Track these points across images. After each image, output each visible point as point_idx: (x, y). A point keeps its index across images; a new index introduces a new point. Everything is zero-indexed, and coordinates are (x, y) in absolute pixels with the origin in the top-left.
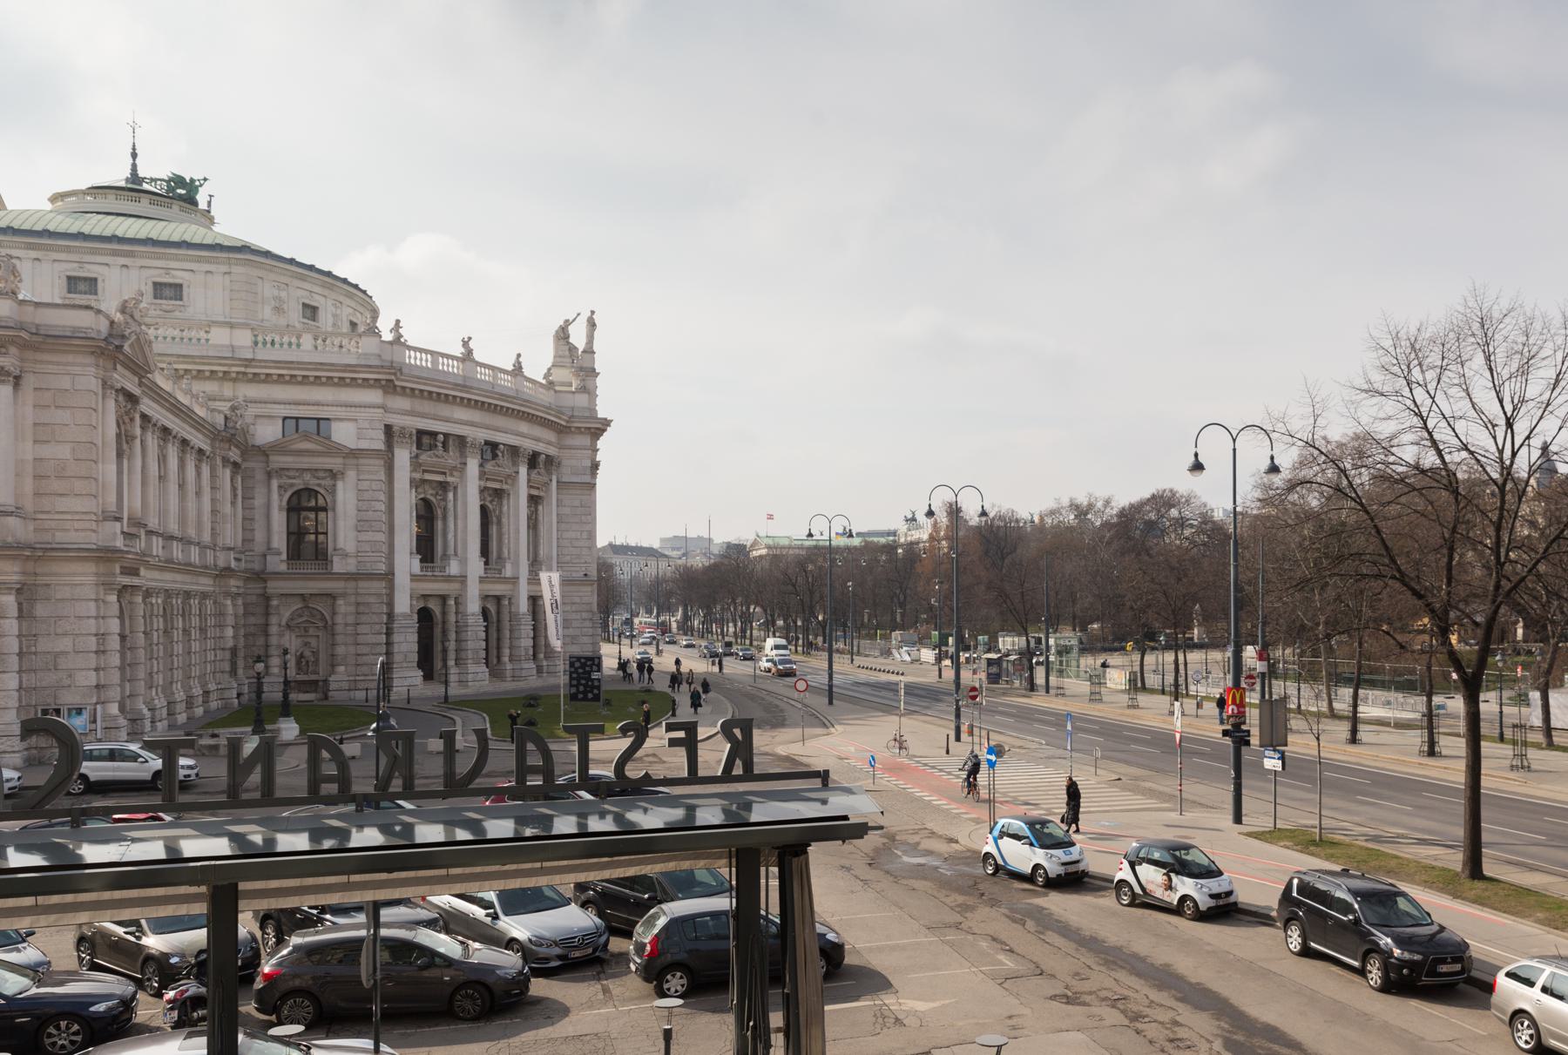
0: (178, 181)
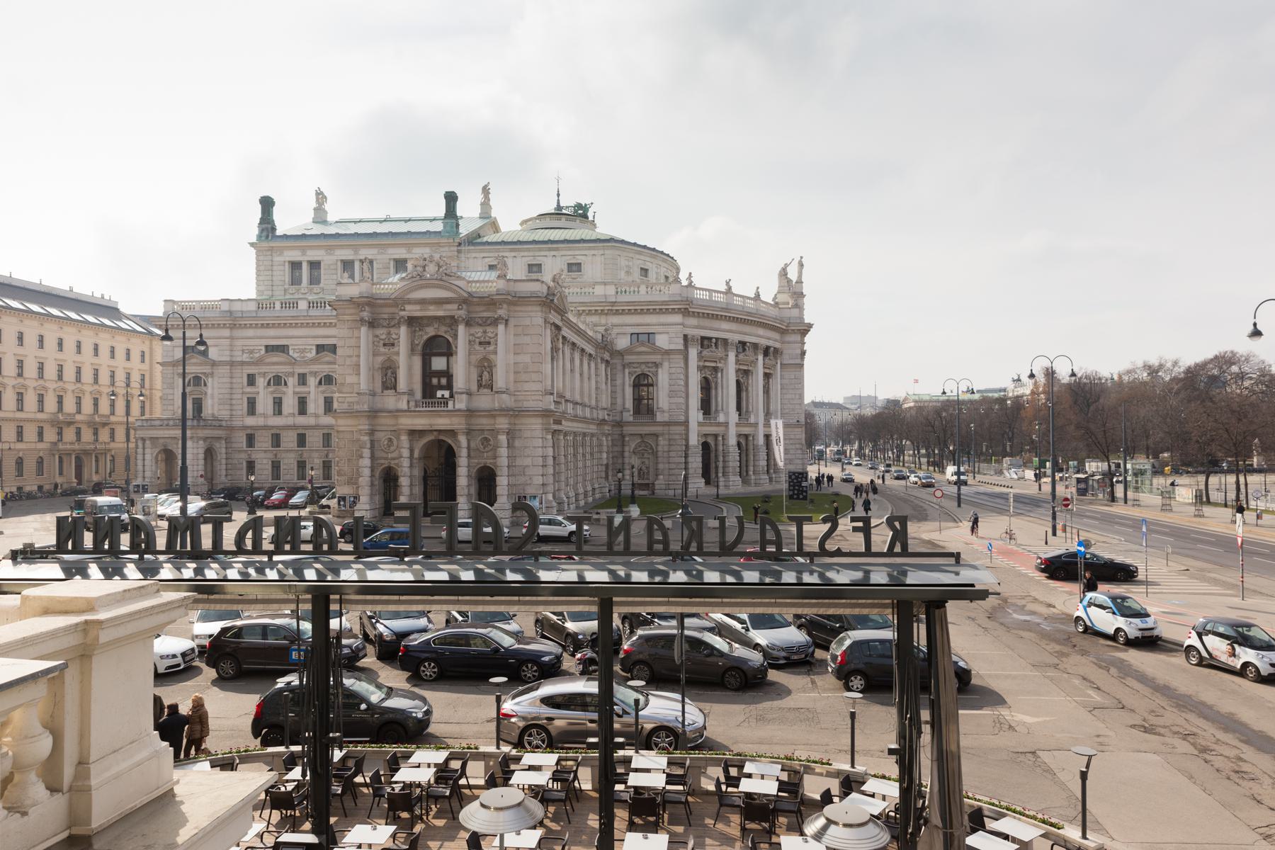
0: (579, 206)
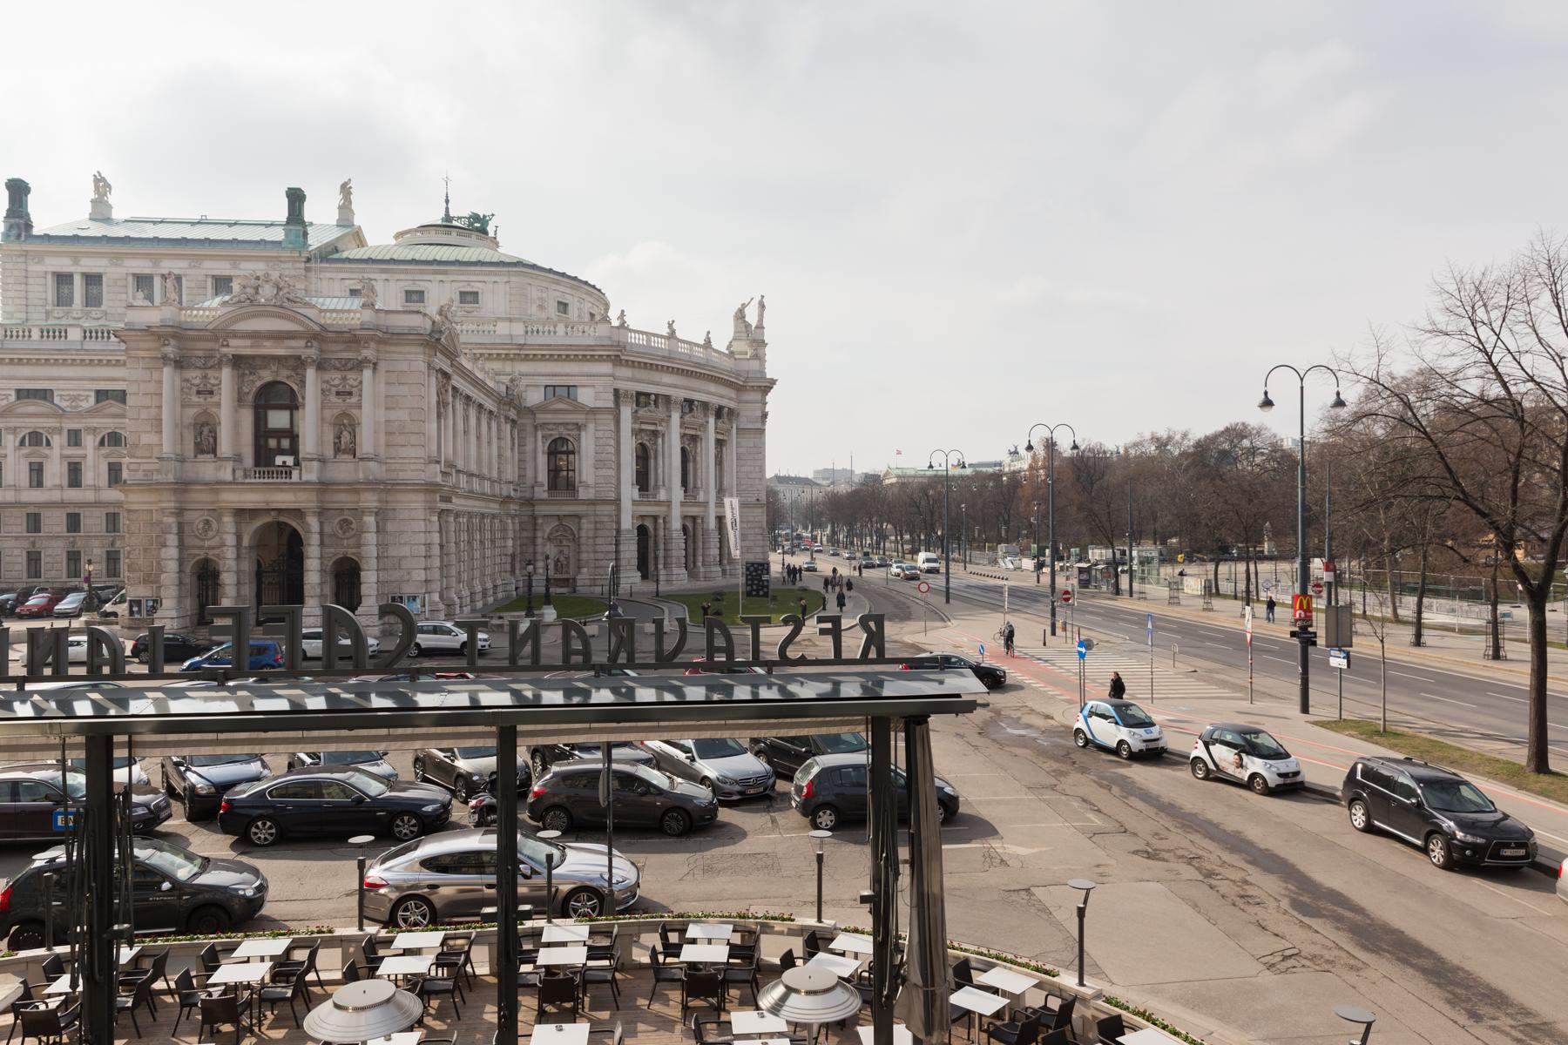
0: (476, 217)
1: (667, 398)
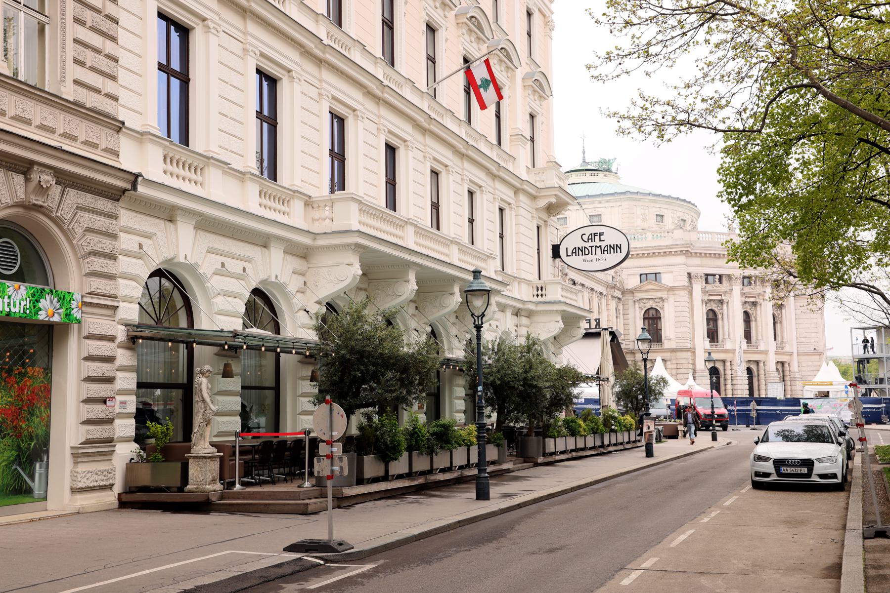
0: (604, 162)
1: (729, 277)
